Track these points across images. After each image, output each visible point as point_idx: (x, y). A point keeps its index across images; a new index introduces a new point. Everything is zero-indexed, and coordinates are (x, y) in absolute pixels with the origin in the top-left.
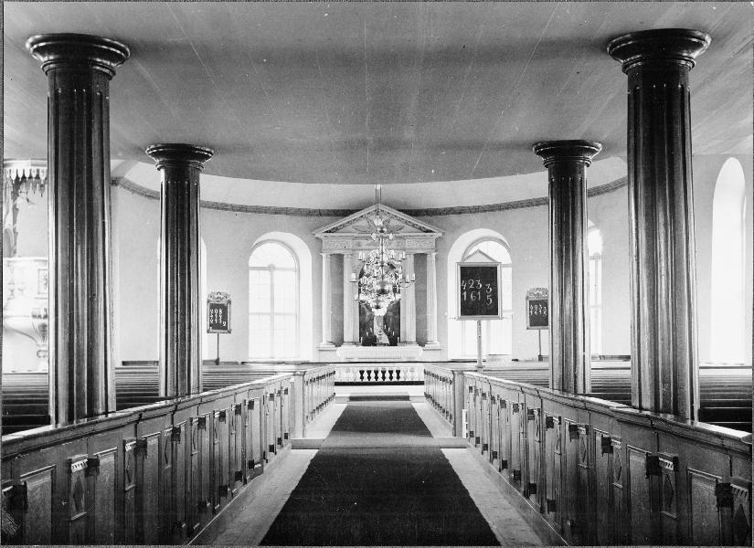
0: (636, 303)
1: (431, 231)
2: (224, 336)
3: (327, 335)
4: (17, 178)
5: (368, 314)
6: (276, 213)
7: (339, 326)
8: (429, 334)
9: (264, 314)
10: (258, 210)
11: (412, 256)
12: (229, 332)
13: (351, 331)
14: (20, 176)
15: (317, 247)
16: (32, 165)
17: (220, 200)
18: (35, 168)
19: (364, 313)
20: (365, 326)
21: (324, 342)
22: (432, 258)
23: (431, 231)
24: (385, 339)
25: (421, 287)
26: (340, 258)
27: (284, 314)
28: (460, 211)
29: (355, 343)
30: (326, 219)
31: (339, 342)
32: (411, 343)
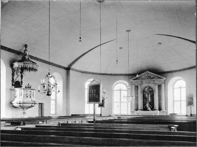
0: (28, 103)
1: (162, 78)
2: (102, 108)
3: (134, 108)
4: (29, 67)
5: (145, 102)
6: (120, 75)
7: (137, 105)
8: (162, 108)
9: (125, 102)
10: (115, 75)
11: (157, 85)
12: (104, 107)
13: (140, 106)
14: (30, 67)
15: (131, 84)
16: (18, 64)
17: (104, 73)
18: (24, 65)
19: (144, 101)
20: (144, 104)
21: (133, 110)
22: (163, 86)
23: (162, 78)
24: (149, 109)
25: (137, 96)
26: (137, 86)
27: (124, 102)
28: (171, 72)
29: (141, 110)
30: (157, 78)
31: (137, 109)
32: (157, 110)
